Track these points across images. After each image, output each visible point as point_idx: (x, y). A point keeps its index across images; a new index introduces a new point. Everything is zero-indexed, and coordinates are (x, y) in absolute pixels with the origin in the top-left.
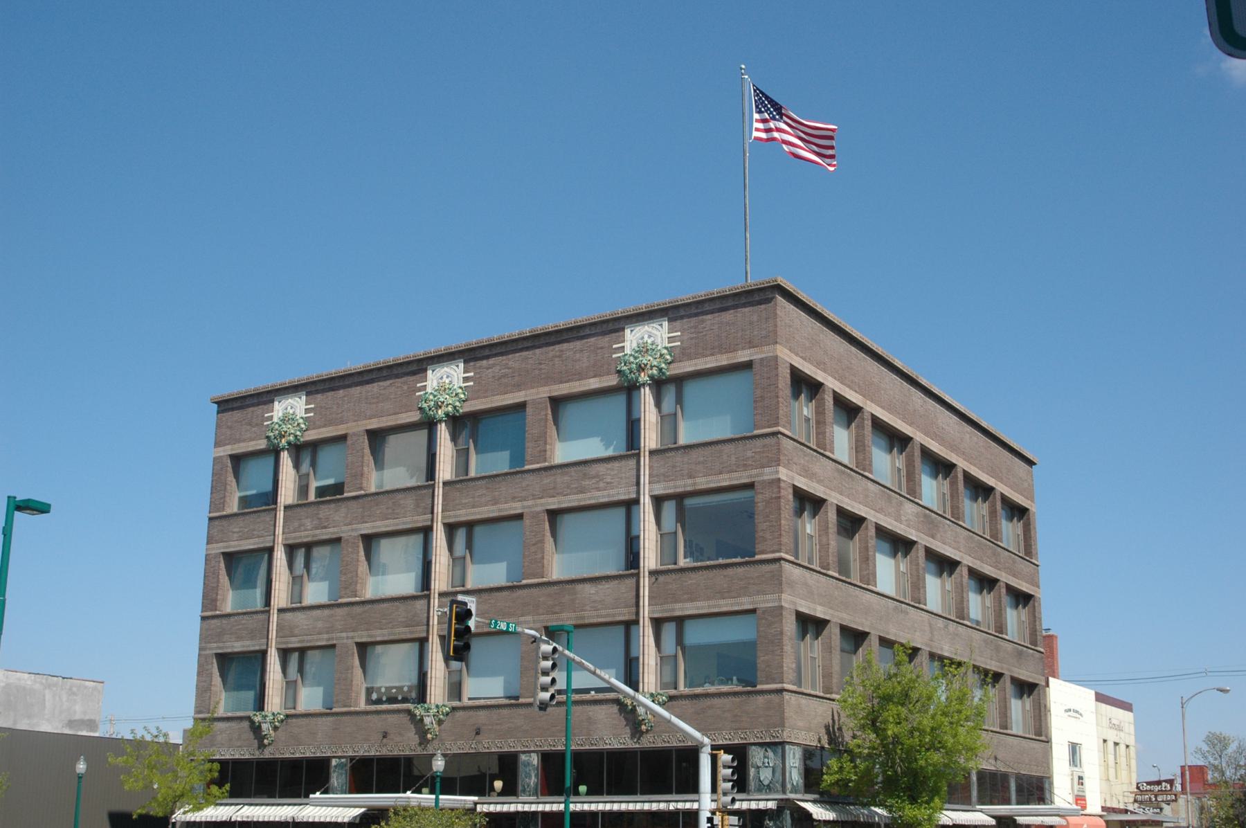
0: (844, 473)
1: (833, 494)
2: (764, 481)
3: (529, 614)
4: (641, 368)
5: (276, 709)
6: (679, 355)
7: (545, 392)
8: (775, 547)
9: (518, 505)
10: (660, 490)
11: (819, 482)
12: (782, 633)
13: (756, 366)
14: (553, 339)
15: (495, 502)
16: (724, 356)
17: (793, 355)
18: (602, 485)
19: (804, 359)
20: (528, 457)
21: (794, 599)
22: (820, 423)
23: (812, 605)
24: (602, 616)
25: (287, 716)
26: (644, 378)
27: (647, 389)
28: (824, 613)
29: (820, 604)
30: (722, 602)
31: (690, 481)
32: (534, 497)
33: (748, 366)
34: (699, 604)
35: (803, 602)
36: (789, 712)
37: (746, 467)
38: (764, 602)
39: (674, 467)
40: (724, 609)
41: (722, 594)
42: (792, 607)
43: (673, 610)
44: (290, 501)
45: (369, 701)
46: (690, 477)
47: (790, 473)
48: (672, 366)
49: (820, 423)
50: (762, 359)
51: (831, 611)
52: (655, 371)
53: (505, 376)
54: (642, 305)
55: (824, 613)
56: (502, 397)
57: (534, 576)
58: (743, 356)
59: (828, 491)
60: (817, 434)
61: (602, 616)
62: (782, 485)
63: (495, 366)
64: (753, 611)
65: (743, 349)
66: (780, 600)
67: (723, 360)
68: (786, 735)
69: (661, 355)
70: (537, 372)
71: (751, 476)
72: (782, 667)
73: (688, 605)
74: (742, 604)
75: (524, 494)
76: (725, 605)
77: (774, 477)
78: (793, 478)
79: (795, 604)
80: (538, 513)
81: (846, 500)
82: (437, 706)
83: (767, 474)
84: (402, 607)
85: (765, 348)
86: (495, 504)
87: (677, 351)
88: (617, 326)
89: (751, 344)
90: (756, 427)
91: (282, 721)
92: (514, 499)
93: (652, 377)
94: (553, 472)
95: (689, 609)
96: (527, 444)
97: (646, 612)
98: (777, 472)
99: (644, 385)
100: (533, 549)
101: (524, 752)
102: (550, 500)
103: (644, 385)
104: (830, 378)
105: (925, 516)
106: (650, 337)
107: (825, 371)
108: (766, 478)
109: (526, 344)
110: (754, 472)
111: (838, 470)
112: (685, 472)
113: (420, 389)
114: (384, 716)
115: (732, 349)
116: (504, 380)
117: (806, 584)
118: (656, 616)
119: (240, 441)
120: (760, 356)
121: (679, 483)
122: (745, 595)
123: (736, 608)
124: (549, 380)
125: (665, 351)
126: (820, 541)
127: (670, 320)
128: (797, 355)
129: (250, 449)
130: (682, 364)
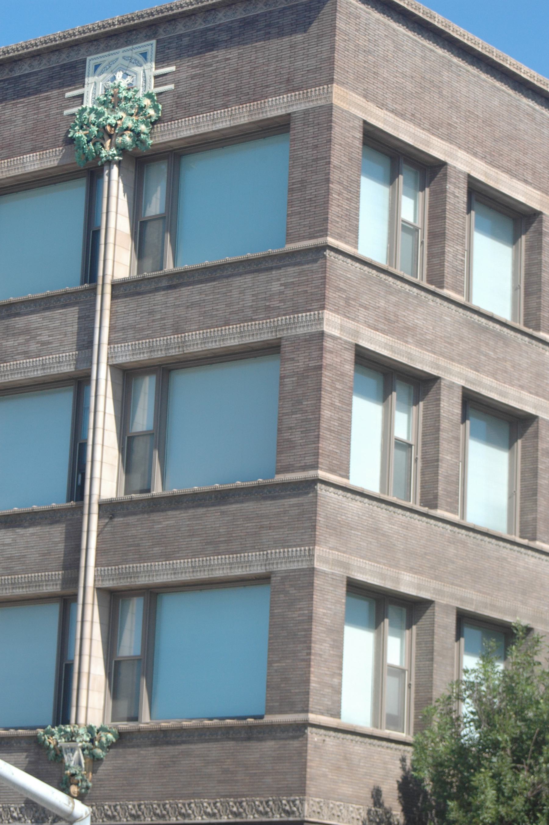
0: (485, 330)
1: (456, 367)
2: (297, 337)
4: (106, 133)
5: (96, 721)
6: (175, 106)
8: (309, 460)
10: (127, 356)
11: (421, 343)
12: (310, 619)
13: (297, 127)
16: (246, 108)
17: (371, 107)
19: (401, 115)
21: (343, 557)
22: (437, 234)
23: (390, 572)
25: (121, 736)
26: (108, 151)
27: (115, 170)
28: (419, 587)
29: (411, 570)
30: (215, 560)
31: (174, 339)
33: (279, 127)
34: (178, 563)
35: (367, 565)
36: (316, 766)
37: (269, 312)
38: (282, 561)
39: (151, 313)
40: (219, 574)
41: (213, 545)
42: (338, 571)
43: (136, 574)
46: (177, 330)
47: (350, 324)
49: (437, 234)
50: (306, 112)
51: (434, 584)
52: (127, 139)
55: (419, 587)
58: (275, 107)
59: (443, 362)
60: (431, 256)
62: (328, 344)
64: (263, 579)
65: (276, 93)
66: (311, 556)
67: (241, 116)
69: (141, 109)
71: (277, 329)
72: (307, 682)
73: (158, 565)
74: (249, 563)
76: (220, 567)
77: (314, 329)
78: (356, 334)
79: (346, 566)
81: (487, 380)
82: (90, 730)
85: (313, 92)
87: (169, 101)
88: (74, 57)
89: (290, 85)
90: (290, 238)
91: (111, 746)
93: (122, 150)
95: (160, 572)
98: (320, 320)
103: (109, 163)
104: (461, 154)
107: (449, 138)
108: (301, 331)
110: (282, 320)
111: (472, 325)
112: (169, 322)
115: (257, 94)
117: (376, 530)
118: (108, 584)
120: (303, 107)
121: (160, 341)
122: (254, 548)
123: (238, 572)
125: (147, 102)
126: (424, 453)
128: (382, 106)
130: (174, 124)
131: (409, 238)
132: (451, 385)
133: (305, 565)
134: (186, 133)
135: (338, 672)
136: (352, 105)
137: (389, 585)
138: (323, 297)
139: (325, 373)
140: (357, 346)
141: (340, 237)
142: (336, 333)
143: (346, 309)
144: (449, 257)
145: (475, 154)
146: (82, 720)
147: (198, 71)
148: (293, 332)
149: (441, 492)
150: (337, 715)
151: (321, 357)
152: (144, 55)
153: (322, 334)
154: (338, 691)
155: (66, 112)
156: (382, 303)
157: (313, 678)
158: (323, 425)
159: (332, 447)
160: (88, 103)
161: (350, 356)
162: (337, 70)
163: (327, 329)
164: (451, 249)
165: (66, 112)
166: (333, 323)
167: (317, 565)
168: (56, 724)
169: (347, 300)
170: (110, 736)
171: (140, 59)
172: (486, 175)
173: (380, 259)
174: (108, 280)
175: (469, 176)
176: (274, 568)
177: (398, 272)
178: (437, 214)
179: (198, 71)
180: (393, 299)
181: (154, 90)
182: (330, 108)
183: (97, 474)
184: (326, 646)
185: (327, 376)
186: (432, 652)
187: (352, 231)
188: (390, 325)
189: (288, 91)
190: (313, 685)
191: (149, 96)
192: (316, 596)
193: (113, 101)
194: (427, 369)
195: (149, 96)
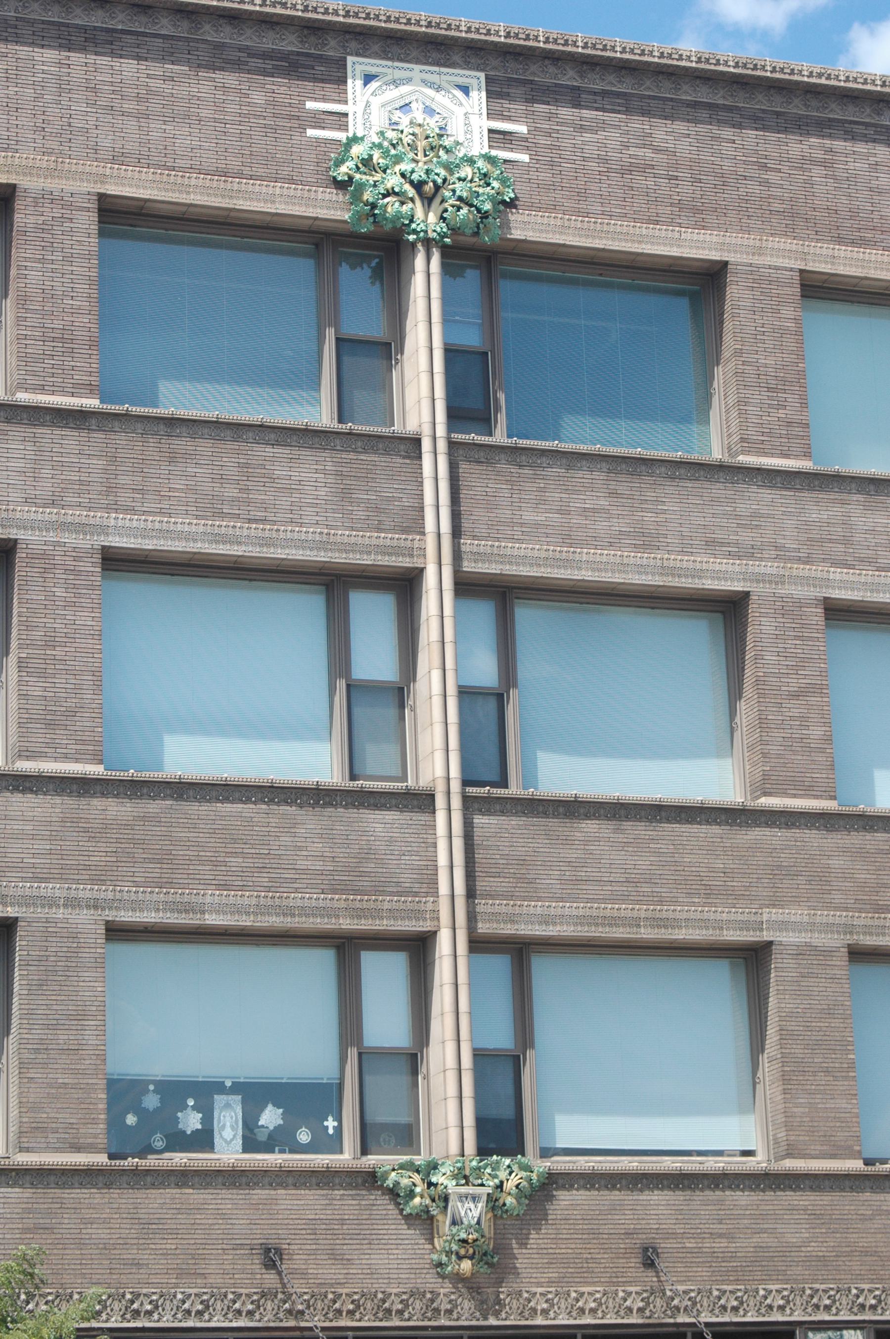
3: (796, 901)
9: (733, 566)
14: (796, 108)
24: (289, 912)
32: (781, 554)
45: (250, 1144)
53: (645, 168)
56: (644, 230)
57: (808, 791)
61: (289, 912)
63: (604, 136)
70: (755, 188)
75: (746, 537)
80: (800, 604)
84: (309, 821)
92: (711, 545)
94: (181, 444)
100: (794, 709)
109: (704, 95)
113: (319, 120)
114: (260, 1194)
116: (639, 181)
123: (647, 934)
124: (794, 220)
127: (496, 91)
129: (124, 194)
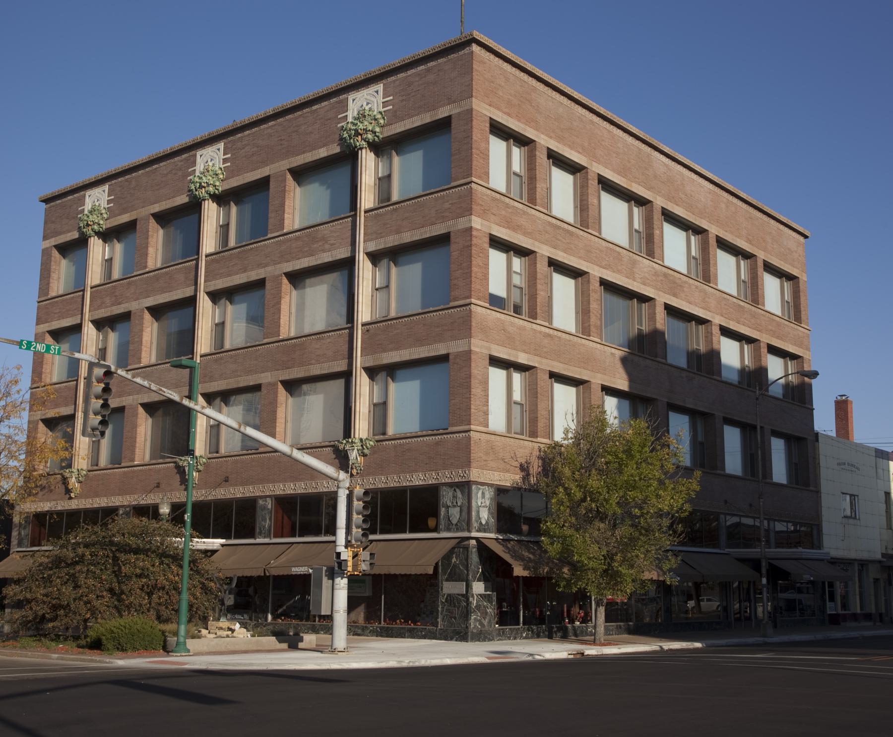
5: (364, 435)
7: (285, 164)
10: (372, 247)
12: (469, 376)
15: (245, 270)
18: (327, 246)
19: (509, 115)
20: (270, 227)
31: (397, 237)
32: (275, 263)
37: (444, 219)
44: (97, 281)
48: (386, 129)
50: (459, 113)
54: (360, 74)
59: (537, 243)
62: (474, 233)
65: (444, 105)
68: (475, 474)
69: (376, 120)
72: (470, 409)
82: (361, 440)
83: (462, 223)
86: (245, 271)
89: (451, 101)
96: (270, 215)
97: (359, 361)
98: (470, 221)
99: (361, 149)
101: (261, 497)
102: (285, 264)
105: (665, 275)
106: (368, 104)
110: (450, 223)
115: (434, 108)
119: (60, 233)
120: (457, 111)
128: (499, 109)
130: (393, 126)
131: (518, 179)
132: (543, 255)
133: (466, 349)
134: (399, 130)
135: (486, 403)
136: (483, 109)
137: (512, 359)
138: (471, 209)
139: (473, 248)
140: (490, 234)
141: (480, 177)
142: (479, 227)
143: (483, 215)
144: (538, 190)
145: (551, 137)
146: (357, 436)
147: (404, 98)
148: (457, 228)
149: (538, 311)
150: (487, 426)
151: (471, 240)
152: (377, 92)
153: (471, 227)
154: (486, 413)
155: (339, 125)
156: (503, 212)
157: (472, 407)
158: (473, 275)
159: (478, 287)
160: (350, 119)
161: (487, 240)
162: (474, 91)
163: (474, 225)
164: (540, 186)
165: (339, 125)
166: (477, 222)
167: (473, 348)
168: (344, 439)
169: (484, 211)
170: (372, 443)
171: (375, 94)
172: (557, 147)
173: (503, 190)
174: (363, 209)
175: (548, 148)
176: (451, 351)
177: (512, 196)
178: (531, 163)
179: (404, 98)
180: (510, 210)
181: (382, 110)
182: (472, 109)
183: (360, 309)
184: (479, 390)
185: (474, 250)
186: (537, 393)
187: (619, 408)
188: (508, 224)
189: (449, 104)
190: (473, 410)
191: (380, 113)
192: (473, 364)
193: (361, 116)
194: (529, 247)
195: (380, 113)
